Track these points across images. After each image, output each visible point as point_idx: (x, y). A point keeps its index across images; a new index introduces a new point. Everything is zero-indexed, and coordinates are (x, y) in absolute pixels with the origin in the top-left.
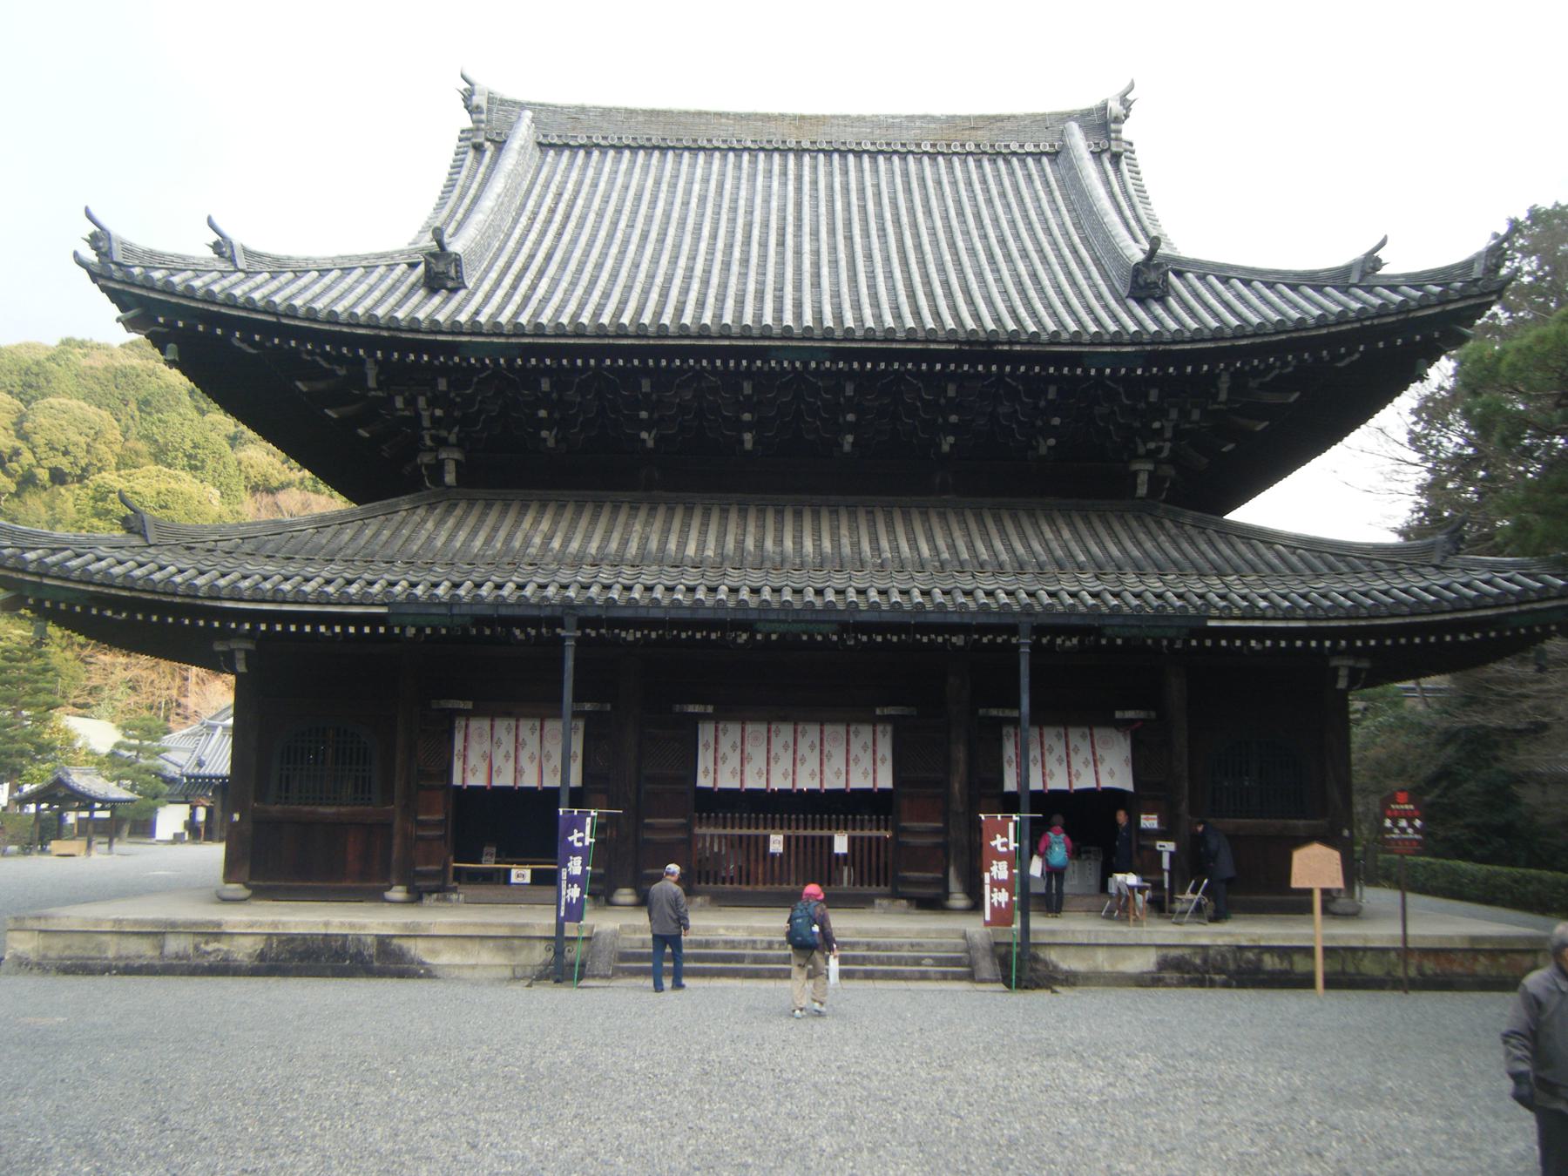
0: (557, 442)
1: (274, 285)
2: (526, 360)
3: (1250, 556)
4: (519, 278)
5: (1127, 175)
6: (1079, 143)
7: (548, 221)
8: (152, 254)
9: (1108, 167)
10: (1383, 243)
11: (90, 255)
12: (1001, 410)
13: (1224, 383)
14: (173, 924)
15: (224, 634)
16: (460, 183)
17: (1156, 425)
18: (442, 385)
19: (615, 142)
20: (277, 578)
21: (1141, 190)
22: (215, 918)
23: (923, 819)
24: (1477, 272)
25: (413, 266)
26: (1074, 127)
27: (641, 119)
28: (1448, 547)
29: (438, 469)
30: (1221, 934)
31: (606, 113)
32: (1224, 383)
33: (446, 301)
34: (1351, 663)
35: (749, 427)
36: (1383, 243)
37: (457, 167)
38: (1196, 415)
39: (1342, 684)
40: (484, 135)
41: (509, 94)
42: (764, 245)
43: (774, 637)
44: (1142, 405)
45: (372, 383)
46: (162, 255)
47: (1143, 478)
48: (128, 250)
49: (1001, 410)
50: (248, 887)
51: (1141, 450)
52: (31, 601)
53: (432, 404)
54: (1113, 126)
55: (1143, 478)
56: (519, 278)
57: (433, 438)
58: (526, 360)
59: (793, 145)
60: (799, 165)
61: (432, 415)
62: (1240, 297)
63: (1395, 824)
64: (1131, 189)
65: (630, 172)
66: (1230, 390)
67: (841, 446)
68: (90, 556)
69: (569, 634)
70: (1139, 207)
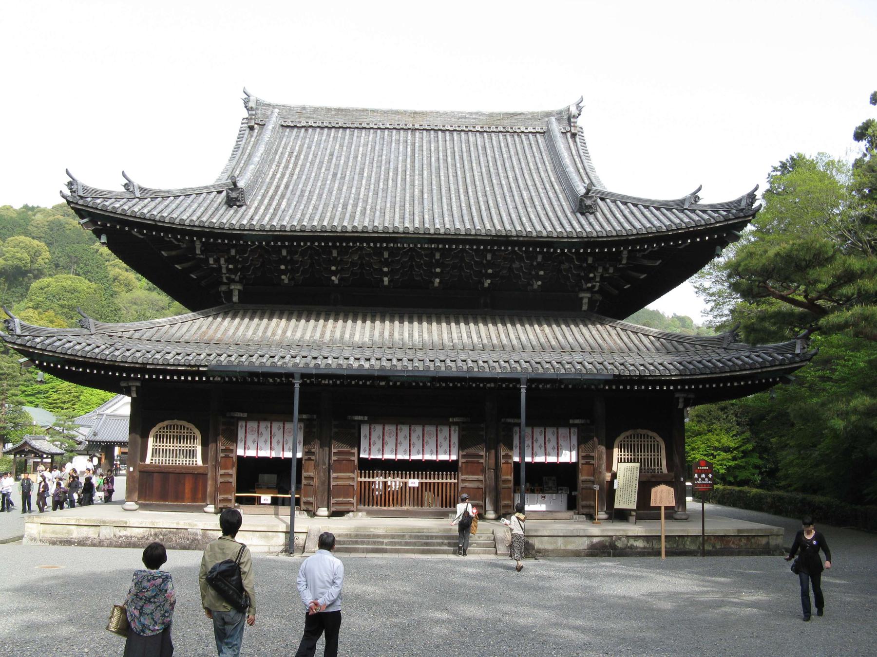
0: (289, 280)
1: (153, 204)
2: (276, 243)
3: (636, 342)
4: (272, 198)
5: (579, 144)
6: (556, 128)
7: (286, 167)
8: (95, 191)
9: (570, 140)
10: (699, 189)
11: (67, 192)
12: (514, 266)
13: (625, 254)
14: (104, 522)
15: (128, 378)
16: (242, 146)
17: (591, 275)
18: (233, 252)
19: (320, 125)
20: (153, 352)
21: (586, 152)
22: (125, 519)
23: (473, 474)
24: (743, 204)
25: (220, 192)
26: (553, 119)
27: (333, 113)
28: (730, 339)
29: (230, 293)
30: (619, 530)
31: (315, 110)
32: (625, 254)
33: (236, 212)
34: (685, 395)
35: (386, 274)
36: (699, 189)
37: (240, 137)
38: (611, 270)
39: (681, 406)
40: (254, 124)
41: (268, 100)
42: (395, 181)
43: (398, 384)
44: (585, 265)
45: (198, 252)
46: (101, 191)
47: (585, 301)
48: (85, 189)
49: (514, 266)
50: (137, 504)
51: (584, 287)
52: (37, 362)
53: (228, 261)
54: (572, 120)
55: (585, 301)
56: (272, 198)
57: (227, 278)
58: (276, 243)
59: (411, 127)
60: (414, 138)
61: (227, 268)
62: (632, 213)
63: (699, 476)
64: (581, 152)
65: (327, 141)
66: (628, 258)
67: (433, 283)
68: (65, 340)
69: (297, 383)
70: (585, 161)
